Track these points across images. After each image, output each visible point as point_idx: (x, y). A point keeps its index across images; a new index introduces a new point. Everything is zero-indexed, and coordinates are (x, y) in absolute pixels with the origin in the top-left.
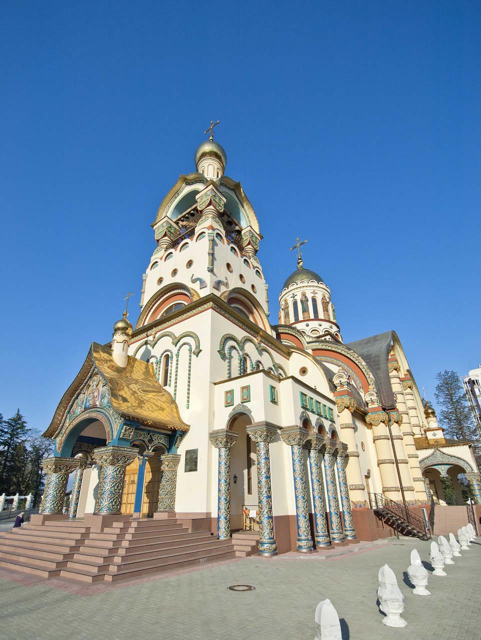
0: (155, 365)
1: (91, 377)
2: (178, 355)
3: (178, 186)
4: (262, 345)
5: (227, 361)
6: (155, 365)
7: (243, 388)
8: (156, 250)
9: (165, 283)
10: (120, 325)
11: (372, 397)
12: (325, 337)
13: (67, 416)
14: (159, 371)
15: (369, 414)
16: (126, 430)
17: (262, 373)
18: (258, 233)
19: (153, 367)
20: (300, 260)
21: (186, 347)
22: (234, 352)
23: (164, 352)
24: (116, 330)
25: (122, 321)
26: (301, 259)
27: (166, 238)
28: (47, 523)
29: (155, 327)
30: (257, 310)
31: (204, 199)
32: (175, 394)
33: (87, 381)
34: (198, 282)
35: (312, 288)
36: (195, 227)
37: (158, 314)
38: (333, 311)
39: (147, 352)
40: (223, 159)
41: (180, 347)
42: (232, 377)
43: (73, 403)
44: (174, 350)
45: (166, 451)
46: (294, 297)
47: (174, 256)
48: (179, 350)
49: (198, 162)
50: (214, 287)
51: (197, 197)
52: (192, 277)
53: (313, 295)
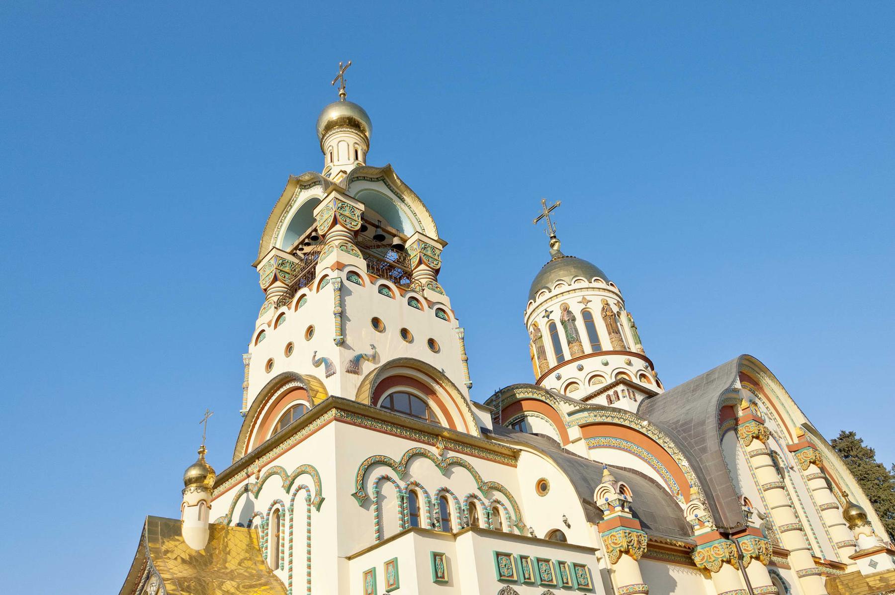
0: (260, 530)
3: (290, 190)
4: (451, 454)
5: (373, 507)
6: (260, 530)
7: (388, 564)
8: (262, 308)
9: (277, 371)
10: (194, 473)
11: (696, 512)
12: (615, 389)
14: (267, 541)
15: (699, 549)
17: (412, 533)
18: (436, 238)
19: (257, 534)
20: (554, 240)
21: (303, 494)
22: (388, 489)
23: (273, 505)
24: (188, 482)
25: (194, 466)
26: (555, 237)
27: (278, 284)
29: (258, 458)
30: (441, 386)
31: (326, 216)
32: (291, 585)
33: (143, 586)
34: (323, 365)
35: (578, 293)
36: (316, 264)
37: (268, 429)
38: (633, 326)
39: (249, 505)
40: (363, 123)
41: (295, 495)
42: (387, 536)
44: (286, 499)
46: (548, 317)
47: (308, 300)
49: (323, 139)
50: (348, 371)
51: (316, 212)
52: (315, 356)
53: (582, 306)
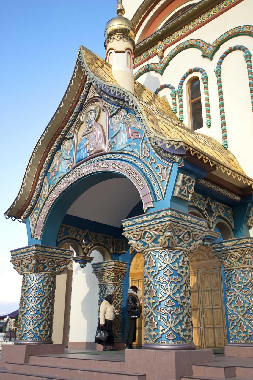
1: (81, 109)
2: (218, 73)
13: (43, 179)
14: (181, 106)
16: (183, 182)
28: (34, 360)
33: (76, 117)
41: (223, 58)
43: (53, 157)
45: (232, 233)
48: (220, 63)
